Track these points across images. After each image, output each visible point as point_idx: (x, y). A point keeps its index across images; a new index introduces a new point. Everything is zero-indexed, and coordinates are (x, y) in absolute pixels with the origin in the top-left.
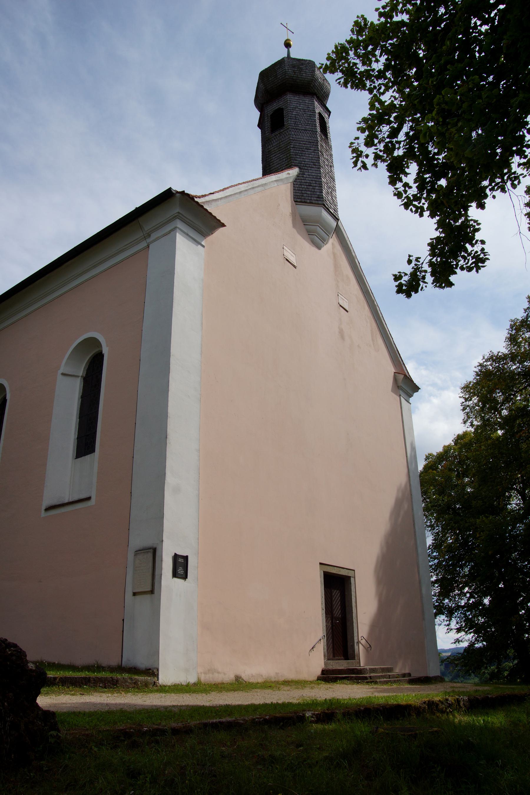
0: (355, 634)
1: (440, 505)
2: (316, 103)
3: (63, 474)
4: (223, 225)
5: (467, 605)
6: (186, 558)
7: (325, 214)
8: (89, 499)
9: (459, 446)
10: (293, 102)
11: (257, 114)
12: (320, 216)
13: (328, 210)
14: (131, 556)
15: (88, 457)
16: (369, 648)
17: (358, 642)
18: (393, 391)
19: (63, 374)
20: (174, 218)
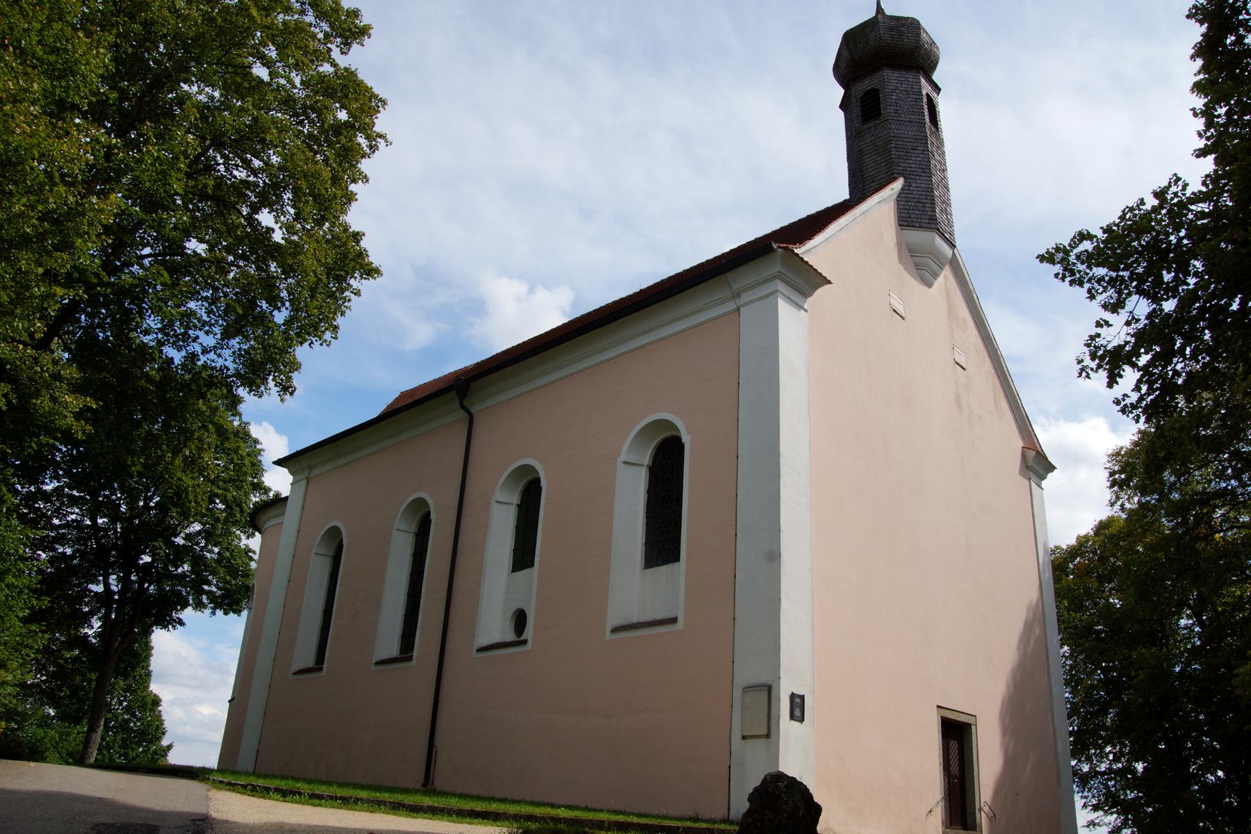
0: (977, 799)
1: (1076, 627)
2: (923, 80)
3: (633, 588)
4: (829, 282)
5: (1110, 771)
6: (802, 697)
7: (939, 241)
8: (673, 620)
9: (1101, 538)
10: (891, 80)
11: (840, 92)
12: (933, 244)
13: (942, 235)
14: (737, 694)
15: (664, 569)
16: (993, 818)
17: (980, 809)
18: (1022, 473)
19: (625, 463)
20: (774, 278)
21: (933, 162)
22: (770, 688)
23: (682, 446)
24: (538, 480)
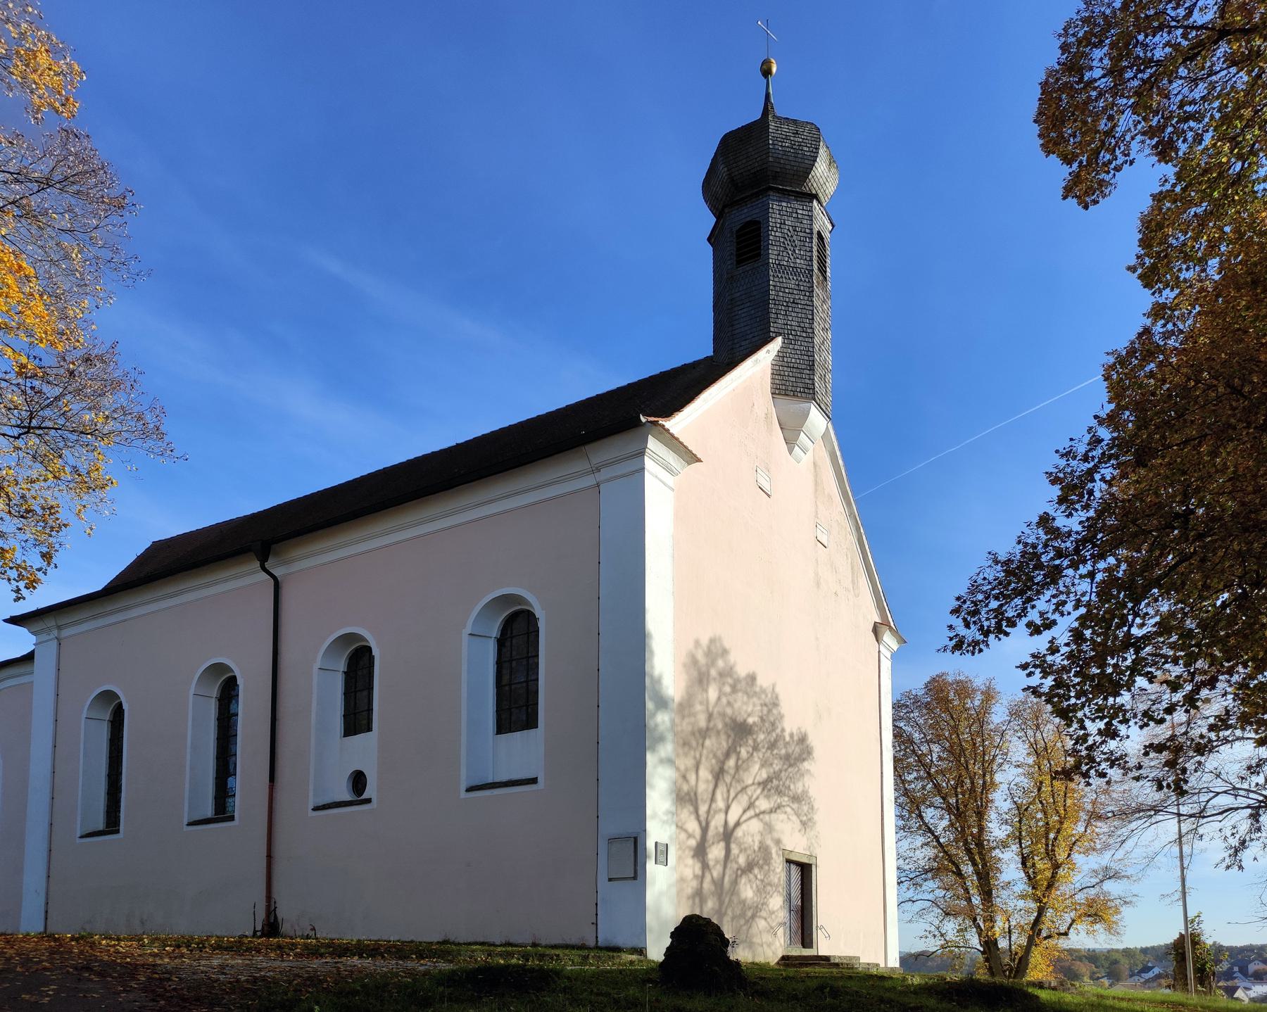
8: (534, 781)
21: (817, 318)
22: (636, 839)
23: (371, 659)
24: (234, 678)
